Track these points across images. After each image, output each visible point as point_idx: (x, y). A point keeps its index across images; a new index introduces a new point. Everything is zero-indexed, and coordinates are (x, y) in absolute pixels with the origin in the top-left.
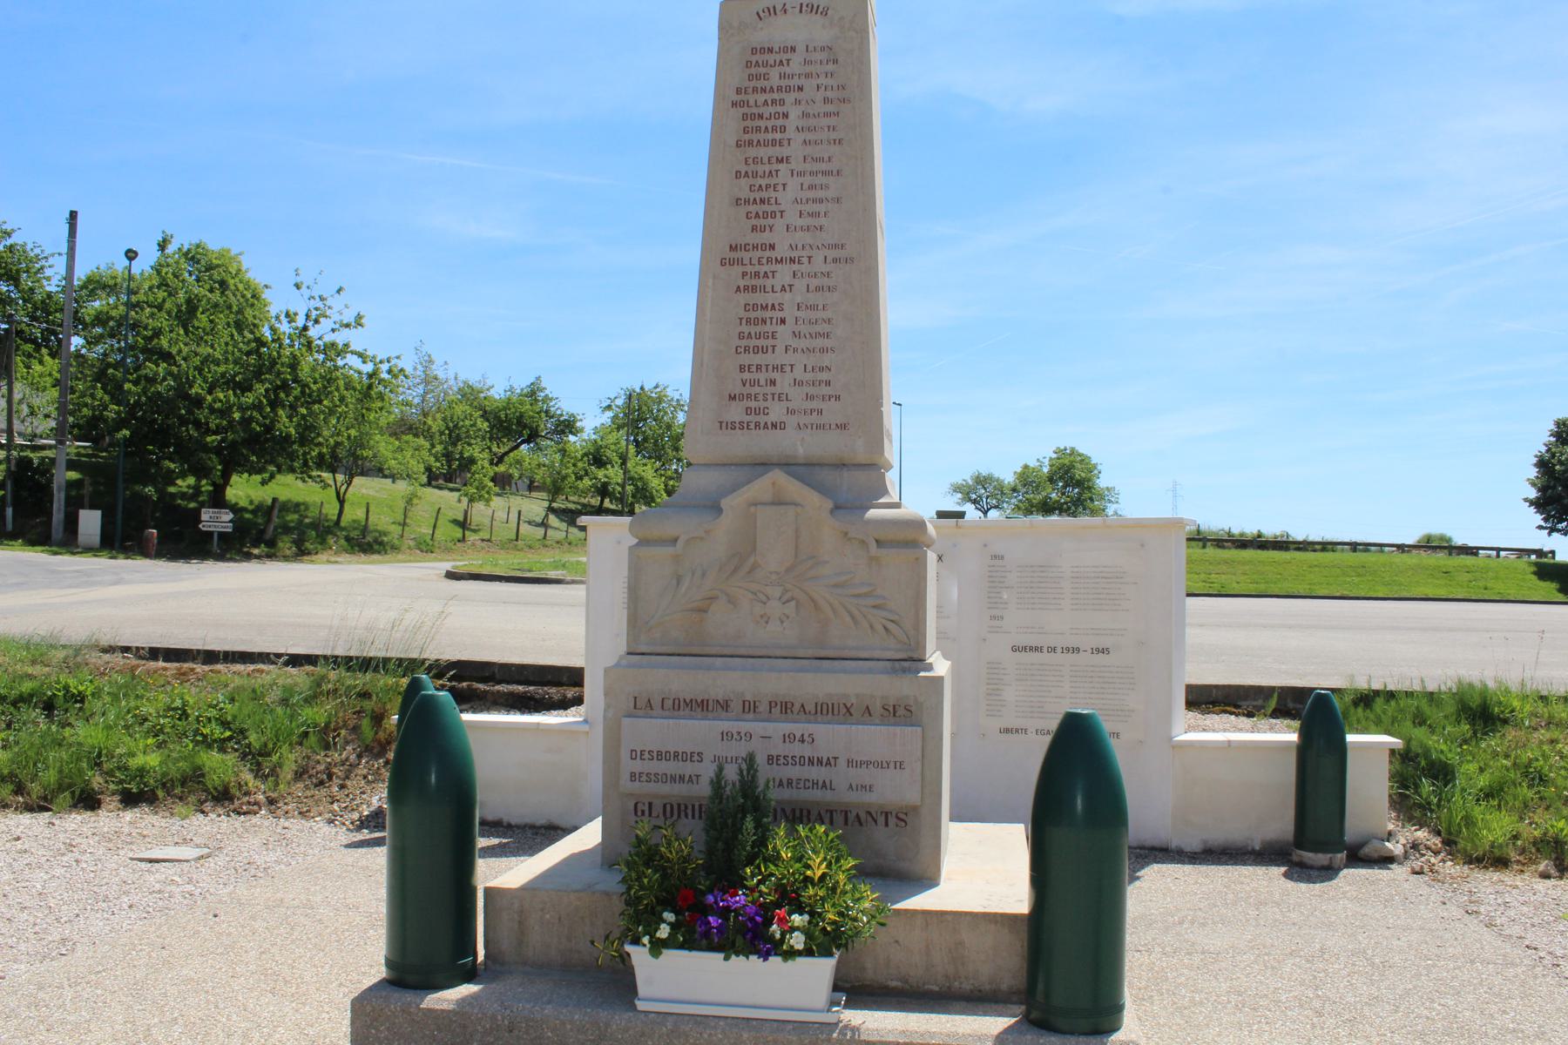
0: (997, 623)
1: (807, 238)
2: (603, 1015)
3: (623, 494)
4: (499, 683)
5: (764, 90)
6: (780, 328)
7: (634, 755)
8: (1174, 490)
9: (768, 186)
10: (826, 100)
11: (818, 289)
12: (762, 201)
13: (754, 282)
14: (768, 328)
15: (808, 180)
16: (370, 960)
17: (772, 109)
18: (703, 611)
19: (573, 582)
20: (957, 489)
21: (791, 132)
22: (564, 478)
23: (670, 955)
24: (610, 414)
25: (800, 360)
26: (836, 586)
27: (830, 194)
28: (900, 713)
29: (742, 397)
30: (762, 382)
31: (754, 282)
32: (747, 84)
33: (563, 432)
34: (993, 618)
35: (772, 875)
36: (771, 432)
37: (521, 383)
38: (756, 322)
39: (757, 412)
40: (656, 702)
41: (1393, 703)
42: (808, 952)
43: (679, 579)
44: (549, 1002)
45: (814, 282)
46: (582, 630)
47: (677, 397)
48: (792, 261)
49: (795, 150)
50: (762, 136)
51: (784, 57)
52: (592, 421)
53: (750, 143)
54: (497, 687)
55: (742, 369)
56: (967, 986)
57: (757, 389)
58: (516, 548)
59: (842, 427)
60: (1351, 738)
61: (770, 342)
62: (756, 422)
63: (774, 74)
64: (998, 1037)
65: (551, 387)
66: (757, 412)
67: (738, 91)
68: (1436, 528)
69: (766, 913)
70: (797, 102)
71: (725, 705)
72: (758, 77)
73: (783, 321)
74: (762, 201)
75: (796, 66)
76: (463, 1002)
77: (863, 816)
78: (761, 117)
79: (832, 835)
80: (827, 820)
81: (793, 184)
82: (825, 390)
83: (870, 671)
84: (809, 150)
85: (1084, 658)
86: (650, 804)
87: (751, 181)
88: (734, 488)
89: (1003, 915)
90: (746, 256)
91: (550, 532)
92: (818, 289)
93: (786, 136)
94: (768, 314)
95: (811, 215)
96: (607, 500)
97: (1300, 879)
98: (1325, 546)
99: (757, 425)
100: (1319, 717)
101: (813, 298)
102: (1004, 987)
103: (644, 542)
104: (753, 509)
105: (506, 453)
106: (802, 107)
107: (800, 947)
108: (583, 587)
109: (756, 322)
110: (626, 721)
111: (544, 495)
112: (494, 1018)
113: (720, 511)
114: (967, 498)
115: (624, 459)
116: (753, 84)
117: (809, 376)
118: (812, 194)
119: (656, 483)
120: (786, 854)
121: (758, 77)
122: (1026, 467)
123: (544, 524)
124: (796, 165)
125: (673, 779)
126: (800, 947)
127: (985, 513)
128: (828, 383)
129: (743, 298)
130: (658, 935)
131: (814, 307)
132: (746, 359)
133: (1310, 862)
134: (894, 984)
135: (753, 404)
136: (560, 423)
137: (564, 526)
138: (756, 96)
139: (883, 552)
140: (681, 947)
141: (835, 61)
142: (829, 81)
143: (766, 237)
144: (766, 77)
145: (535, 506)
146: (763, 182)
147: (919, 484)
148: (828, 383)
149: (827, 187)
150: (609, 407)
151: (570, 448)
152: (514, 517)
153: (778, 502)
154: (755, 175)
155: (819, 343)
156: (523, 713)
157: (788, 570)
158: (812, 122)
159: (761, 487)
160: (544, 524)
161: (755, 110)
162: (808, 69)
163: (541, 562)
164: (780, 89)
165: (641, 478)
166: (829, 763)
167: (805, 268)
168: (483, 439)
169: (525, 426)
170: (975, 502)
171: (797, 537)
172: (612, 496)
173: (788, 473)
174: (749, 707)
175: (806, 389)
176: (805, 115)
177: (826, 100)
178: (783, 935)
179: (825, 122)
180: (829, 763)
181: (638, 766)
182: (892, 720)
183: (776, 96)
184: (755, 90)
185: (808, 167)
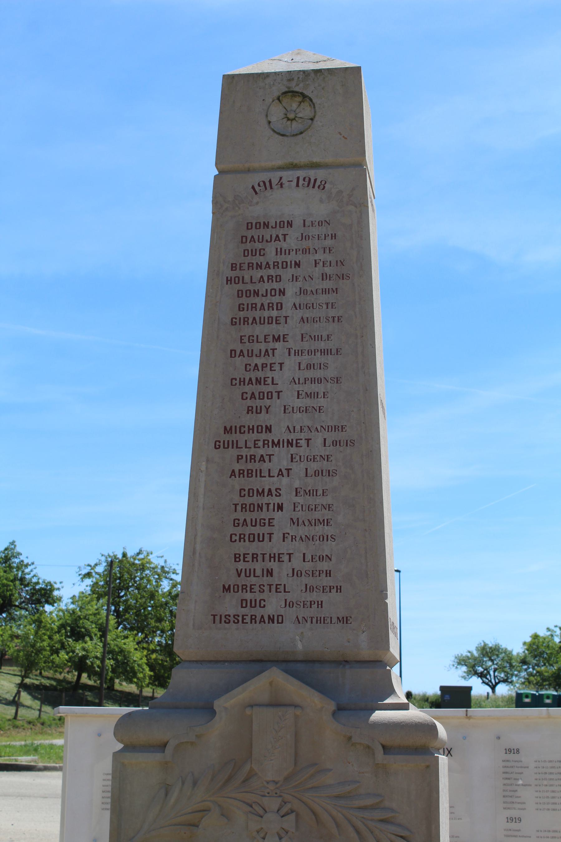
0: (513, 825)
3: (102, 667)
5: (259, 266)
9: (264, 366)
10: (324, 277)
11: (317, 473)
12: (258, 381)
13: (250, 466)
14: (264, 515)
15: (305, 359)
17: (267, 286)
19: (46, 769)
20: (461, 661)
21: (288, 310)
22: (39, 651)
26: (338, 797)
27: (330, 373)
30: (259, 572)
31: (250, 466)
32: (242, 259)
33: (38, 602)
34: (511, 819)
36: (269, 626)
38: (252, 508)
39: (253, 604)
45: (314, 466)
46: (54, 827)
48: (290, 443)
49: (292, 328)
50: (257, 314)
51: (281, 232)
52: (70, 589)
53: (245, 320)
55: (237, 558)
57: (253, 580)
59: (344, 620)
63: (270, 249)
65: (26, 552)
66: (253, 604)
67: (233, 267)
70: (295, 278)
72: (253, 253)
74: (258, 381)
75: (292, 242)
78: (256, 293)
81: (291, 362)
82: (326, 581)
84: (307, 328)
87: (246, 360)
88: (228, 688)
90: (241, 439)
92: (317, 473)
93: (283, 313)
94: (266, 500)
95: (309, 395)
96: (85, 675)
99: (253, 619)
101: (311, 482)
103: (129, 748)
104: (248, 711)
106: (299, 284)
108: (60, 774)
109: (252, 508)
111: (16, 669)
113: (213, 713)
114: (473, 672)
115: (104, 631)
117: (308, 566)
118: (310, 374)
119: (138, 657)
121: (253, 253)
122: (536, 636)
123: (15, 703)
127: (493, 688)
128: (328, 573)
129: (237, 483)
131: (312, 493)
132: (241, 548)
135: (248, 596)
136: (34, 592)
137: (36, 704)
138: (251, 272)
141: (334, 236)
142: (328, 257)
143: (263, 419)
144: (261, 252)
146: (259, 361)
147: (422, 664)
148: (328, 573)
149: (326, 366)
150: (89, 575)
151: (46, 619)
153: (276, 703)
154: (251, 354)
155: (319, 529)
157: (287, 779)
158: (309, 299)
159: (258, 687)
160: (15, 703)
161: (251, 287)
164: (276, 265)
165: (122, 651)
167: (303, 451)
170: (481, 675)
172: (91, 672)
173: (286, 671)
175: (305, 580)
176: (302, 292)
177: (324, 277)
179: (323, 298)
183: (272, 272)
184: (250, 266)
185: (306, 345)
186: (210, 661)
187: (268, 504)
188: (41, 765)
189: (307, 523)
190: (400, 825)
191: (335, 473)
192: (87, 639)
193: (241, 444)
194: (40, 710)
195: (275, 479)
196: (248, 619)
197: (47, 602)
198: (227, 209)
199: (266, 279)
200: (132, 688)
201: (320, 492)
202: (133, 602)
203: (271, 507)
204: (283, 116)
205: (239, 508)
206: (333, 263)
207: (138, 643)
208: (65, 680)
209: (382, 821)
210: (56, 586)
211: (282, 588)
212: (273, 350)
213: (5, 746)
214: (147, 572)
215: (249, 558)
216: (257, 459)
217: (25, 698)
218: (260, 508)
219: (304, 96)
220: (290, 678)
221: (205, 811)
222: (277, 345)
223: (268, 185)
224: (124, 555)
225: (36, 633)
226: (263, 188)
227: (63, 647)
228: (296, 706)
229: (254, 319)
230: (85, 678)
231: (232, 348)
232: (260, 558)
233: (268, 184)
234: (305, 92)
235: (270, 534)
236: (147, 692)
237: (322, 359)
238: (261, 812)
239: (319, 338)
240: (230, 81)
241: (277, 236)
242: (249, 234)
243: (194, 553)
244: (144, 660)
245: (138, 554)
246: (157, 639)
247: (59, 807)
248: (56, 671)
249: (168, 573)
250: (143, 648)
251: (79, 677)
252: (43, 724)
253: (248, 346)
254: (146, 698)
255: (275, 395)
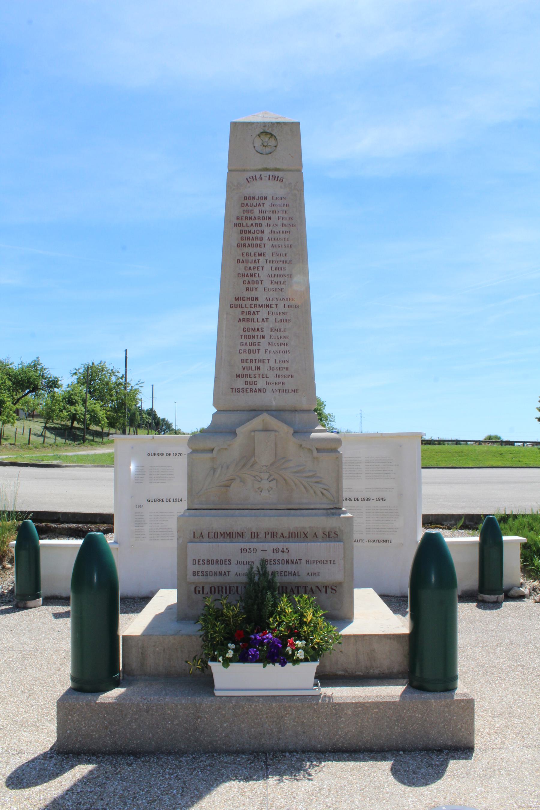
1: (272, 295)
2: (198, 699)
3: (84, 419)
4: (62, 523)
6: (262, 341)
7: (194, 562)
8: (361, 415)
9: (254, 268)
10: (283, 225)
11: (281, 321)
12: (251, 275)
13: (248, 317)
14: (256, 340)
15: (274, 265)
16: (62, 678)
17: (255, 228)
18: (228, 486)
19: (66, 466)
21: (265, 241)
23: (234, 666)
24: (76, 377)
25: (272, 357)
26: (296, 472)
28: (331, 536)
29: (243, 376)
30: (253, 368)
31: (248, 317)
32: (242, 215)
33: (51, 387)
35: (283, 621)
37: (28, 361)
38: (249, 337)
39: (251, 383)
40: (205, 534)
41: (517, 521)
42: (306, 660)
43: (214, 470)
44: (166, 694)
45: (279, 317)
47: (111, 368)
49: (268, 250)
50: (250, 242)
51: (261, 202)
52: (67, 381)
53: (244, 245)
54: (62, 525)
55: (242, 361)
56: (377, 672)
57: (250, 372)
58: (28, 448)
59: (295, 391)
60: (504, 538)
61: (257, 348)
62: (251, 388)
64: (401, 696)
65: (45, 363)
66: (251, 383)
67: (238, 218)
68: (493, 433)
69: (284, 640)
70: (269, 225)
71: (241, 535)
72: (248, 212)
73: (263, 337)
74: (251, 275)
75: (267, 206)
76: (120, 697)
77: (314, 589)
79: (312, 599)
80: (296, 592)
81: (267, 266)
82: (286, 373)
83: (316, 515)
84: (274, 250)
85: (373, 503)
86: (203, 587)
87: (245, 265)
89: (394, 635)
90: (243, 303)
91: (46, 440)
92: (281, 321)
94: (256, 333)
95: (276, 283)
96: (75, 423)
97: (485, 608)
98: (440, 442)
99: (251, 390)
100: (490, 529)
101: (278, 325)
102: (395, 671)
103: (195, 451)
104: (253, 434)
105: (21, 398)
106: (271, 228)
107: (302, 657)
108: (108, 473)
110: (190, 545)
111: (42, 420)
112: (138, 705)
115: (84, 401)
116: (245, 215)
117: (278, 365)
118: (277, 272)
119: (101, 414)
120: (289, 610)
121: (248, 212)
124: (269, 257)
125: (216, 574)
126: (302, 657)
128: (287, 369)
129: (242, 325)
130: (227, 656)
131: (279, 330)
133: (488, 600)
134: (340, 673)
135: (249, 379)
136: (49, 382)
137: (53, 436)
138: (247, 221)
139: (320, 454)
140: (239, 661)
141: (287, 205)
142: (285, 215)
143: (254, 294)
144: (252, 211)
145: (37, 426)
146: (252, 265)
148: (287, 369)
149: (285, 269)
150: (75, 374)
152: (27, 432)
153: (266, 430)
154: (247, 262)
155: (283, 348)
156: (77, 539)
157: (272, 464)
158: (276, 236)
159: (257, 422)
161: (247, 229)
162: (273, 208)
163: (48, 455)
164: (259, 218)
165: (93, 411)
166: (297, 563)
167: (274, 310)
168: (9, 390)
169: (31, 383)
171: (276, 447)
172: (79, 421)
173: (272, 416)
174: (255, 535)
175: (276, 372)
176: (272, 232)
177: (283, 225)
178: (293, 651)
179: (283, 236)
180: (297, 563)
181: (197, 568)
182: (328, 539)
183: (257, 221)
184: (246, 218)
185: (275, 258)
186: (223, 411)
187: (257, 336)
188: (64, 464)
189: (276, 345)
190: (324, 484)
191: (290, 321)
192: (77, 405)
193: (244, 306)
194: (55, 439)
195: (260, 323)
196: (249, 390)
197: (55, 387)
198: (234, 189)
199: (254, 225)
200: (98, 428)
201: (283, 330)
202: (97, 387)
203: (259, 337)
204: (261, 144)
205: (243, 337)
206: (287, 219)
207: (101, 407)
208: (66, 425)
209: (316, 482)
210: (60, 379)
211: (265, 376)
212: (259, 260)
213: (45, 456)
214: (104, 372)
215: (249, 361)
216: (252, 313)
217: (48, 434)
218: (253, 337)
219: (272, 135)
220: (272, 418)
221: (232, 480)
222: (260, 258)
223: (254, 178)
224: (93, 364)
225: (52, 402)
226: (252, 179)
227: (65, 408)
228: (275, 431)
229: (249, 244)
230: (75, 424)
231: (238, 258)
232: (254, 361)
233: (254, 178)
234: (273, 133)
235: (259, 350)
236: (106, 430)
237: (283, 265)
238: (260, 480)
239: (281, 255)
240: (235, 126)
241: (259, 204)
242: (245, 202)
243: (221, 359)
244: (105, 415)
245: (100, 363)
246: (110, 405)
247: (113, 484)
248: (61, 420)
249: (115, 372)
250: (104, 409)
251: (72, 423)
252: (57, 446)
253: (245, 258)
254: (105, 433)
255: (260, 282)
